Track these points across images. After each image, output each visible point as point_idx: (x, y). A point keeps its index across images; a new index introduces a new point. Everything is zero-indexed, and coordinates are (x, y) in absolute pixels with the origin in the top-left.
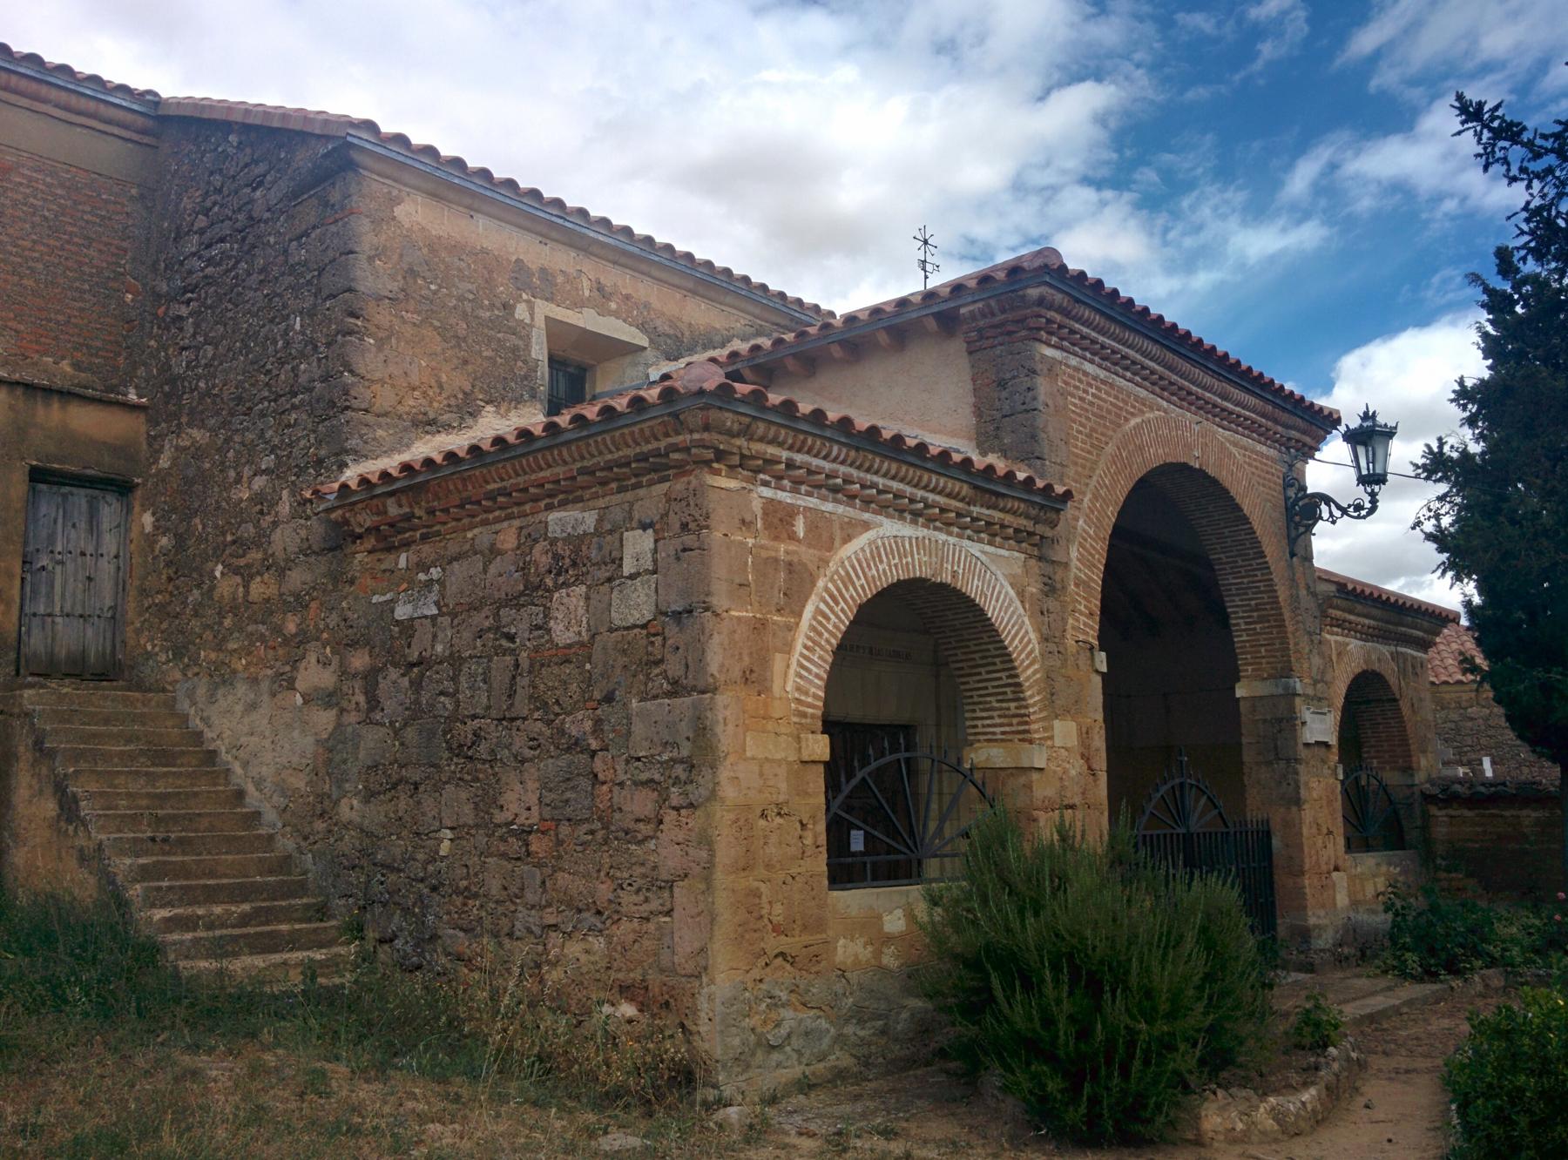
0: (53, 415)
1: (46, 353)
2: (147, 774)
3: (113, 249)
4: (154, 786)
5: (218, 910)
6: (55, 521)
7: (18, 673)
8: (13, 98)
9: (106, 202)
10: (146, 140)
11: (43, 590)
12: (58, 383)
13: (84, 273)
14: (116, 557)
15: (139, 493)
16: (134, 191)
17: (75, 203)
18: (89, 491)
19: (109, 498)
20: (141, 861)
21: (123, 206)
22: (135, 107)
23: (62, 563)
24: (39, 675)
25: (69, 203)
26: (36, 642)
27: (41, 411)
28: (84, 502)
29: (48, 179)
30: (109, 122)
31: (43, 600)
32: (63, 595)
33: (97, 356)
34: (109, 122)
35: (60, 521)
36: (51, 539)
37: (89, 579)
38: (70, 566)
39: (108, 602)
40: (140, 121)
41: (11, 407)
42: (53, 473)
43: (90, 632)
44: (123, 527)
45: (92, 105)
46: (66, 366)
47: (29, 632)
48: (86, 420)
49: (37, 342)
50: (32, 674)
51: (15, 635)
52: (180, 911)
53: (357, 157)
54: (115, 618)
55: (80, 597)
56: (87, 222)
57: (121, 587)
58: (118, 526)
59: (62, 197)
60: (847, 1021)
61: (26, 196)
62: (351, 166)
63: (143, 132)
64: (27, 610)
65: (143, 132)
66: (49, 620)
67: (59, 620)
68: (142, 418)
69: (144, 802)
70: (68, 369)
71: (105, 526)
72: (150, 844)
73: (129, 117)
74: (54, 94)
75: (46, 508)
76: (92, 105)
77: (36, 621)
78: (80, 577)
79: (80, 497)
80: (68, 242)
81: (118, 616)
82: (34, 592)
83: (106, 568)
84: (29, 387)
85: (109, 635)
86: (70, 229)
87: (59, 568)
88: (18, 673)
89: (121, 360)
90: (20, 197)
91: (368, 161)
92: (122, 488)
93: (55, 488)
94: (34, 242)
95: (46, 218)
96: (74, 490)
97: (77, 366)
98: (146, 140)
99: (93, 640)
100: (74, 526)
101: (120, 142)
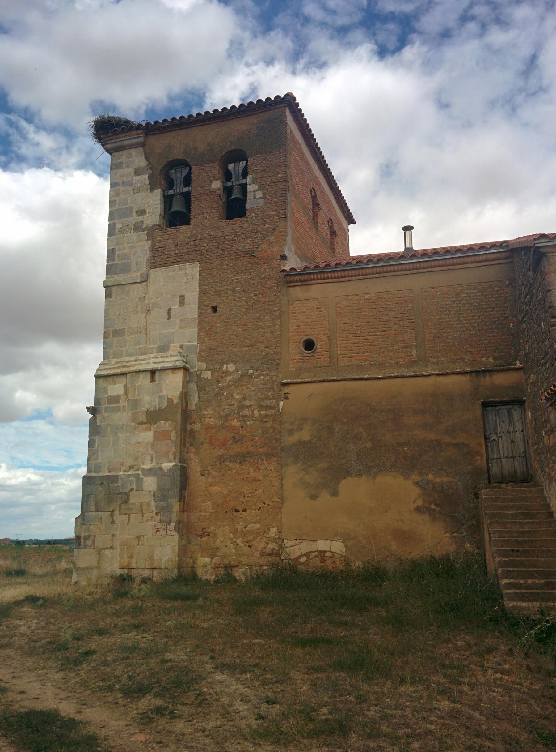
0: (487, 380)
1: (483, 357)
2: (520, 523)
3: (502, 308)
4: (523, 528)
5: (530, 581)
6: (496, 421)
7: (490, 482)
8: (456, 267)
9: (497, 291)
10: (508, 261)
11: (495, 449)
12: (489, 367)
13: (492, 322)
14: (522, 431)
15: (527, 403)
16: (507, 283)
17: (485, 296)
18: (507, 407)
19: (515, 407)
20: (504, 559)
21: (504, 290)
22: (501, 250)
23: (501, 437)
24: (498, 482)
25: (483, 297)
26: (495, 469)
27: (482, 379)
28: (505, 411)
29: (474, 291)
30: (493, 260)
31: (496, 453)
32: (503, 450)
33: (502, 352)
34: (493, 260)
35: (498, 420)
36: (495, 428)
37: (513, 442)
38: (504, 438)
39: (522, 450)
40: (504, 255)
41: (471, 381)
42: (490, 402)
43: (517, 463)
44: (523, 418)
45: (484, 257)
46: (491, 360)
47: (492, 466)
48: (500, 379)
49: (479, 354)
50: (495, 483)
51: (486, 467)
52: (513, 580)
53: (542, 250)
54: (526, 456)
55: (510, 449)
56: (491, 301)
57: (526, 442)
58: (521, 418)
59: (480, 296)
60: (109, 592)
61: (467, 300)
62: (543, 255)
63: (506, 258)
64: (491, 457)
65: (506, 258)
66: (499, 460)
67: (503, 460)
68: (522, 372)
69: (515, 535)
70: (492, 361)
71: (516, 419)
72: (512, 552)
73: (499, 255)
74: (469, 259)
75: (491, 416)
76: (484, 257)
77: (494, 461)
78: (509, 441)
79: (504, 410)
80: (485, 312)
81: (527, 455)
82: (492, 450)
83: (519, 435)
84: (476, 372)
85: (524, 464)
86: (485, 306)
87: (500, 439)
88: (490, 482)
89: (512, 351)
90: (465, 302)
91: (549, 250)
92: (521, 403)
93: (494, 408)
94: (472, 316)
95: (476, 306)
96: (501, 407)
97: (495, 358)
98: (508, 261)
99: (518, 465)
100: (503, 421)
101: (498, 266)
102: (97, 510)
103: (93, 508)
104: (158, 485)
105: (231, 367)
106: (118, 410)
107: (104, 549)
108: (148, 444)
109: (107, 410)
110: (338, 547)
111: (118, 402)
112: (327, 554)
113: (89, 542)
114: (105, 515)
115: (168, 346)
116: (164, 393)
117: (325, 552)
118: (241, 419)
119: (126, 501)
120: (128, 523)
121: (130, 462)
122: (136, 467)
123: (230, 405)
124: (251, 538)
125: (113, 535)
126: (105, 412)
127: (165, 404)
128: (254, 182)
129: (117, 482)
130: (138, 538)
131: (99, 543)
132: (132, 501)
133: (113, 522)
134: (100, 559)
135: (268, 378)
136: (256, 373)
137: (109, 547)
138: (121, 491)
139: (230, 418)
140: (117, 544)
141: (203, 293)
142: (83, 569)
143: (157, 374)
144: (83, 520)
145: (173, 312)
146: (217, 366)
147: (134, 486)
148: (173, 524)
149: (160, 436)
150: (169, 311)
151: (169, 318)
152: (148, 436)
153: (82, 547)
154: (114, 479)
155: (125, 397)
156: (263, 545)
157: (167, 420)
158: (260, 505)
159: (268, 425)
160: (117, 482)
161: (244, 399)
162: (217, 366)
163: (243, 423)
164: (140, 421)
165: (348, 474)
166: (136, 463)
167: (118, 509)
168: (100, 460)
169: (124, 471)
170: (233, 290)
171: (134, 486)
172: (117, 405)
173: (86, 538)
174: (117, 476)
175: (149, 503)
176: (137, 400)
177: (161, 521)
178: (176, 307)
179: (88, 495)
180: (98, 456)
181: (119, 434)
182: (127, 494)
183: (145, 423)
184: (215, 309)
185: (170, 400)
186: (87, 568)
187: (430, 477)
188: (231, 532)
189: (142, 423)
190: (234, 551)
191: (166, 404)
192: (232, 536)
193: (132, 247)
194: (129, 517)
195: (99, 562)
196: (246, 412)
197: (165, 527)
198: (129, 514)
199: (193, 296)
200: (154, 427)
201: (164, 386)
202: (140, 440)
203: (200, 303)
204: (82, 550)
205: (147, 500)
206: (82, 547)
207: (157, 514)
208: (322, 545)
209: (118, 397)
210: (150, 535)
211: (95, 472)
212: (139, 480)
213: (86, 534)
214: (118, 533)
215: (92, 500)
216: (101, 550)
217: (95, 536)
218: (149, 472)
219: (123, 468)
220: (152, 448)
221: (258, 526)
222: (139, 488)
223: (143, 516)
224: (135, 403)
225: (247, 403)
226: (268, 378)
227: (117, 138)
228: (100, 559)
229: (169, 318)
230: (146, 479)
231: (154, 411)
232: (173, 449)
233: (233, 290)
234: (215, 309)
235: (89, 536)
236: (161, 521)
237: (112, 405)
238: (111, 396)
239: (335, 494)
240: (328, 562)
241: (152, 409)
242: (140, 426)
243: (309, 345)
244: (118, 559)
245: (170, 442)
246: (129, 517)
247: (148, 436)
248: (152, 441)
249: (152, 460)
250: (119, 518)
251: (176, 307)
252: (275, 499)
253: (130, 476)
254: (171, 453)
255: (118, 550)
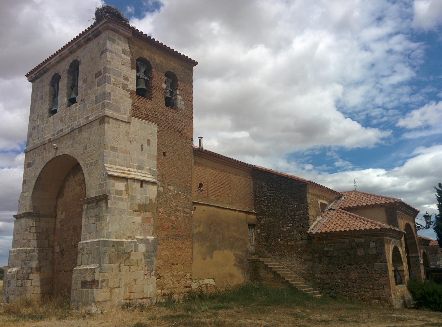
102: (110, 263)
103: (107, 262)
104: (146, 249)
105: (172, 188)
106: (122, 199)
107: (114, 288)
108: (139, 224)
109: (115, 198)
110: (212, 282)
111: (121, 195)
112: (209, 285)
113: (104, 284)
114: (115, 266)
115: (143, 167)
116: (148, 195)
117: (208, 284)
118: (176, 216)
119: (128, 258)
120: (129, 271)
121: (129, 234)
122: (132, 237)
123: (171, 208)
124: (179, 278)
125: (120, 279)
126: (114, 199)
127: (148, 202)
128: (180, 94)
129: (123, 246)
130: (135, 280)
131: (111, 284)
132: (131, 258)
133: (120, 271)
134: (111, 295)
135: (187, 198)
136: (182, 194)
137: (117, 286)
138: (126, 251)
139: (171, 215)
140: (122, 284)
141: (159, 143)
142: (100, 302)
143: (144, 182)
144: (101, 269)
145: (144, 148)
146: (166, 186)
147: (133, 249)
148: (154, 272)
149: (145, 220)
150: (142, 146)
151: (142, 150)
152: (138, 219)
153: (100, 287)
154: (121, 244)
155: (126, 192)
156: (184, 282)
157: (149, 211)
158: (184, 262)
159: (187, 221)
160: (123, 245)
161: (177, 206)
162: (166, 186)
163: (176, 219)
164: (135, 209)
165: (216, 249)
166: (132, 234)
167: (123, 263)
168: (110, 231)
169: (126, 239)
170: (173, 147)
171: (133, 249)
172: (120, 196)
173: (102, 282)
174: (123, 242)
175: (141, 259)
176: (133, 196)
177: (148, 270)
178: (145, 145)
179: (104, 253)
180: (109, 228)
181: (123, 215)
182: (129, 254)
183: (138, 211)
184: (164, 154)
185: (151, 200)
186: (103, 301)
187: (237, 252)
188: (171, 276)
189: (136, 211)
190: (172, 286)
191: (148, 202)
192: (171, 278)
193: (121, 98)
194: (130, 267)
195: (110, 297)
196: (178, 213)
197: (149, 274)
198: (130, 266)
199: (154, 141)
200: (142, 214)
201: (148, 191)
202: (135, 221)
203: (158, 148)
204: (99, 290)
205: (141, 258)
206: (100, 287)
207: (145, 266)
208: (207, 281)
209: (122, 191)
210: (142, 279)
211: (107, 238)
212: (136, 246)
213: (103, 279)
214: (123, 278)
215: (106, 256)
216: (112, 289)
217: (108, 280)
218: (142, 241)
219: (125, 237)
220: (141, 227)
221: (183, 272)
222: (136, 250)
223: (138, 267)
224: (132, 198)
225: (179, 208)
226: (187, 198)
227: (117, 25)
228: (111, 295)
229: (142, 150)
230: (140, 245)
231: (143, 205)
232: (152, 229)
233: (173, 147)
234: (164, 154)
235: (105, 280)
236: (148, 270)
237: (118, 196)
238: (117, 190)
239: (211, 258)
240: (209, 289)
241: (141, 203)
242: (135, 213)
243: (201, 185)
244: (123, 293)
245: (150, 224)
246: (130, 267)
247: (138, 219)
248: (141, 222)
249: (141, 234)
250: (124, 268)
251: (145, 145)
252: (190, 259)
253: (131, 242)
254: (151, 231)
255: (123, 288)
